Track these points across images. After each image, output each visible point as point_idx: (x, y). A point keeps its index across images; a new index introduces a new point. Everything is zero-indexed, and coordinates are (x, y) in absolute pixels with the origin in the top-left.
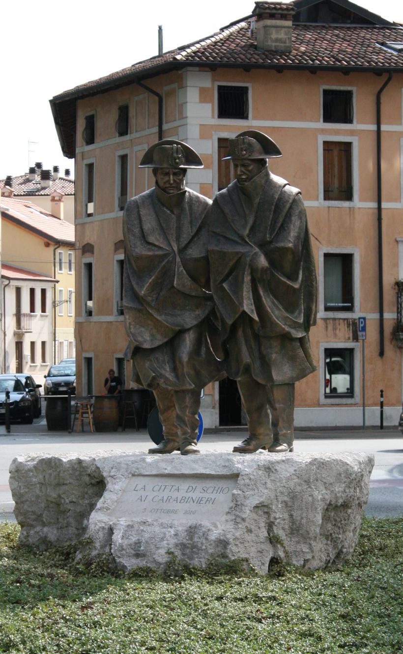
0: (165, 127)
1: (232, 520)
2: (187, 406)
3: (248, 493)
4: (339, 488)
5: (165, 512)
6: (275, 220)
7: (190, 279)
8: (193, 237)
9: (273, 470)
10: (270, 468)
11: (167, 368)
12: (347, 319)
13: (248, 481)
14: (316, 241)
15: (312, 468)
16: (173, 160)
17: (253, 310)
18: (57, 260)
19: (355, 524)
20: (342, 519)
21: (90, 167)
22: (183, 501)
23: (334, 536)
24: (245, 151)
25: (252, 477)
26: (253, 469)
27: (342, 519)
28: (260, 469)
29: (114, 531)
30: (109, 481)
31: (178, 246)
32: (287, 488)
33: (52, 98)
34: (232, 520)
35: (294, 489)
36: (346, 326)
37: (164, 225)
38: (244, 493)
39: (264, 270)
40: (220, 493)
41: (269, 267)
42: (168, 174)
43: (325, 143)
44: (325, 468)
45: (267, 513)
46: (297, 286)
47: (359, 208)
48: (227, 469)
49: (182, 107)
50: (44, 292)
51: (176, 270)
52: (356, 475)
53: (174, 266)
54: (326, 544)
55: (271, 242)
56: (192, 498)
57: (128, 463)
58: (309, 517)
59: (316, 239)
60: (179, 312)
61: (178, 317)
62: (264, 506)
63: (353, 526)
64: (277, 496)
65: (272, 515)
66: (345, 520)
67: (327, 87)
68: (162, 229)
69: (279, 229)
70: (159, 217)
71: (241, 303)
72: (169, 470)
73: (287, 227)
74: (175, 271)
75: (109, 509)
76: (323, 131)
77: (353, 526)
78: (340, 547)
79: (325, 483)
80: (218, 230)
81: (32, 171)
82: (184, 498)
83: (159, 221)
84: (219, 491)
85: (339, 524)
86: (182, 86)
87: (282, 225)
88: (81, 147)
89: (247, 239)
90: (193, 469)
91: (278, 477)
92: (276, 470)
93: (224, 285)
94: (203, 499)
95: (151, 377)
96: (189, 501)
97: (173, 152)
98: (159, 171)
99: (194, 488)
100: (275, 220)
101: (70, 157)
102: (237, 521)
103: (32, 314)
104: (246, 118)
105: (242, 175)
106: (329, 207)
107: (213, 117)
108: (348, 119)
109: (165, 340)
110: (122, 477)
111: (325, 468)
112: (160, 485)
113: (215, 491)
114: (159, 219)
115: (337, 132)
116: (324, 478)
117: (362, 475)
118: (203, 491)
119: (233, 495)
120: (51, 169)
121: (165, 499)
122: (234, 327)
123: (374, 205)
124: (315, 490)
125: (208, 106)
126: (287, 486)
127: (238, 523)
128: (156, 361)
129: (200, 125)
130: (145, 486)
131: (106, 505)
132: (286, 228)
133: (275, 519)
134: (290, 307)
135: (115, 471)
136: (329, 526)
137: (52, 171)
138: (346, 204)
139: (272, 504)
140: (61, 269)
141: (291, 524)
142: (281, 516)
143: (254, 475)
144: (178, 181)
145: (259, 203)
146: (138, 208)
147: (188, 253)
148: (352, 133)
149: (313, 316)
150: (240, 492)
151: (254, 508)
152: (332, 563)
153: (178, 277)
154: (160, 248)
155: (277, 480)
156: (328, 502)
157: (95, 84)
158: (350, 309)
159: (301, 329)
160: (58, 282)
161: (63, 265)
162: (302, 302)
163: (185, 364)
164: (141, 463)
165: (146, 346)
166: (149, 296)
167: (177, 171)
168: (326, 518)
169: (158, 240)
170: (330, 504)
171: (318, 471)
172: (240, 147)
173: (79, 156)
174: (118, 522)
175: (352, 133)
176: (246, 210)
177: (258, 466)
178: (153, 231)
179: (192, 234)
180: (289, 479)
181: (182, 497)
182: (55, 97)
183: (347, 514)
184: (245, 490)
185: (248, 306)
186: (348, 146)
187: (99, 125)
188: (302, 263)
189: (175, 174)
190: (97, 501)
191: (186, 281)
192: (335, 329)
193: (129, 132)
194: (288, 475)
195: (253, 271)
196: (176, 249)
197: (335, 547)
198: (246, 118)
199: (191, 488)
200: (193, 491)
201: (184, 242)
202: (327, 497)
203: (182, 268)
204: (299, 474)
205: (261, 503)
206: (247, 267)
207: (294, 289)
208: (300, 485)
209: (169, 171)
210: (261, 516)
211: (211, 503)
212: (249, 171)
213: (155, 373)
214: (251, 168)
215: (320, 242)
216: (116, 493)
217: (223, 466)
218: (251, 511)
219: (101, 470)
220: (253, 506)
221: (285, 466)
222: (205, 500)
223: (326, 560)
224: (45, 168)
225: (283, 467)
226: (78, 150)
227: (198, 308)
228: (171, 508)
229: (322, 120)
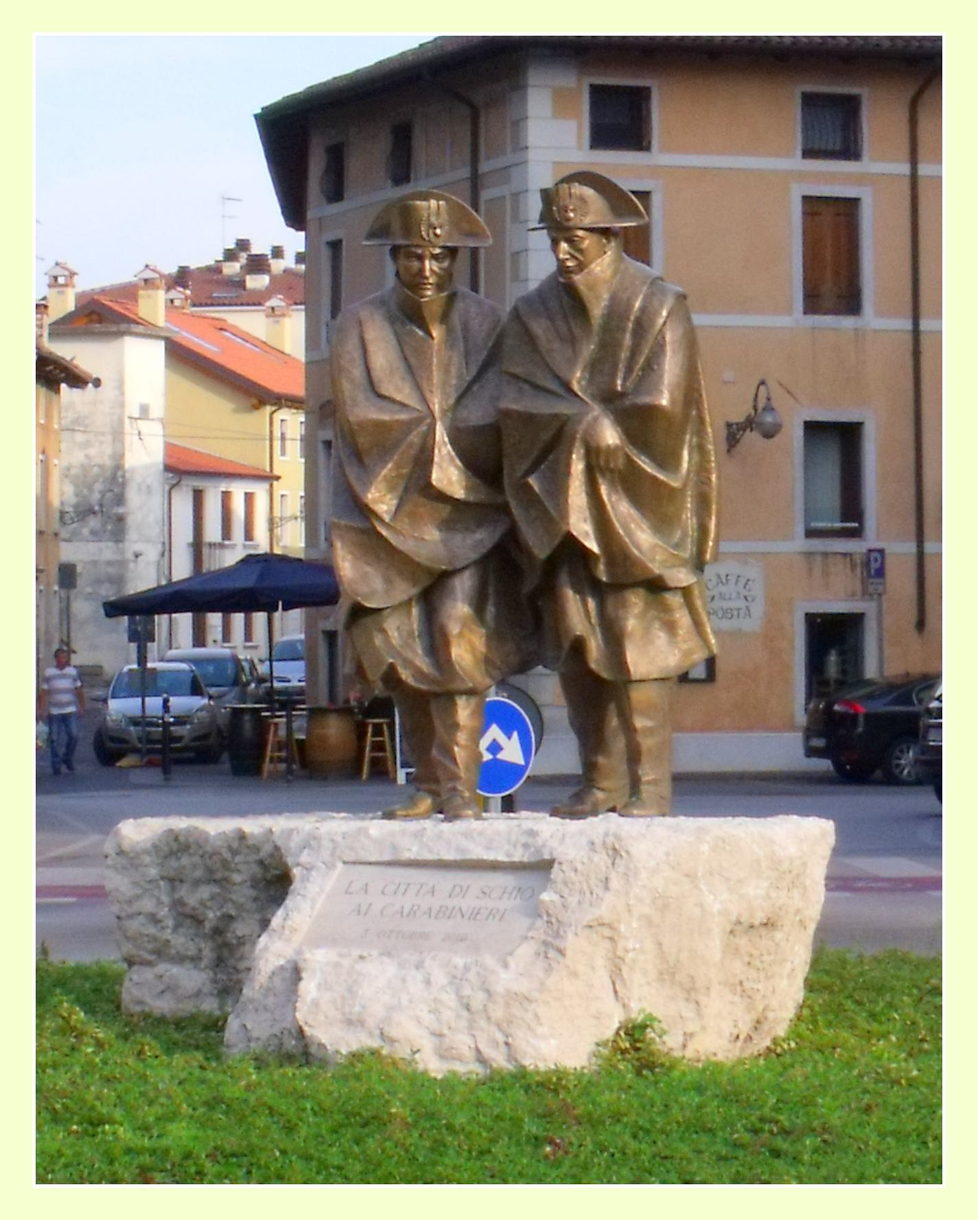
0: (484, 167)
4: (756, 890)
12: (851, 555)
14: (787, 395)
16: (431, 231)
18: (277, 434)
19: (792, 962)
20: (765, 952)
21: (335, 246)
22: (441, 915)
23: (747, 985)
24: (572, 210)
27: (765, 952)
29: (304, 975)
33: (259, 111)
36: (849, 566)
37: (413, 361)
39: (610, 451)
43: (807, 199)
44: (728, 848)
45: (611, 939)
46: (675, 484)
47: (875, 331)
49: (519, 124)
50: (249, 498)
52: (791, 864)
54: (732, 1003)
59: (789, 392)
63: (788, 966)
66: (769, 954)
67: (599, 81)
68: (410, 369)
69: (643, 369)
72: (413, 851)
76: (801, 176)
77: (788, 966)
78: (760, 1008)
79: (728, 880)
80: (518, 370)
81: (230, 255)
85: (758, 963)
86: (520, 87)
88: (316, 207)
90: (463, 851)
93: (532, 481)
94: (482, 911)
98: (402, 251)
101: (298, 229)
103: (227, 542)
104: (648, 148)
106: (814, 328)
107: (580, 147)
108: (850, 151)
111: (728, 848)
113: (506, 895)
115: (832, 178)
117: (804, 864)
118: (481, 895)
120: (268, 252)
121: (406, 911)
122: (552, 566)
123: (907, 325)
125: (572, 124)
129: (554, 163)
130: (367, 885)
132: (655, 367)
133: (627, 951)
134: (662, 521)
136: (738, 966)
137: (270, 257)
138: (847, 322)
140: (283, 453)
148: (860, 179)
152: (745, 1041)
154: (404, 406)
156: (734, 918)
157: (345, 82)
158: (856, 533)
160: (278, 478)
161: (288, 444)
168: (731, 950)
170: (739, 923)
173: (312, 225)
175: (860, 179)
179: (468, 379)
182: (267, 108)
183: (773, 941)
185: (582, 527)
186: (852, 204)
187: (354, 166)
190: (273, 914)
192: (826, 574)
193: (412, 176)
195: (594, 455)
197: (750, 1008)
198: (648, 148)
199: (458, 889)
205: (597, 920)
207: (672, 489)
211: (498, 917)
215: (796, 400)
219: (283, 851)
222: (484, 913)
223: (731, 1034)
224: (255, 250)
226: (311, 214)
229: (799, 153)
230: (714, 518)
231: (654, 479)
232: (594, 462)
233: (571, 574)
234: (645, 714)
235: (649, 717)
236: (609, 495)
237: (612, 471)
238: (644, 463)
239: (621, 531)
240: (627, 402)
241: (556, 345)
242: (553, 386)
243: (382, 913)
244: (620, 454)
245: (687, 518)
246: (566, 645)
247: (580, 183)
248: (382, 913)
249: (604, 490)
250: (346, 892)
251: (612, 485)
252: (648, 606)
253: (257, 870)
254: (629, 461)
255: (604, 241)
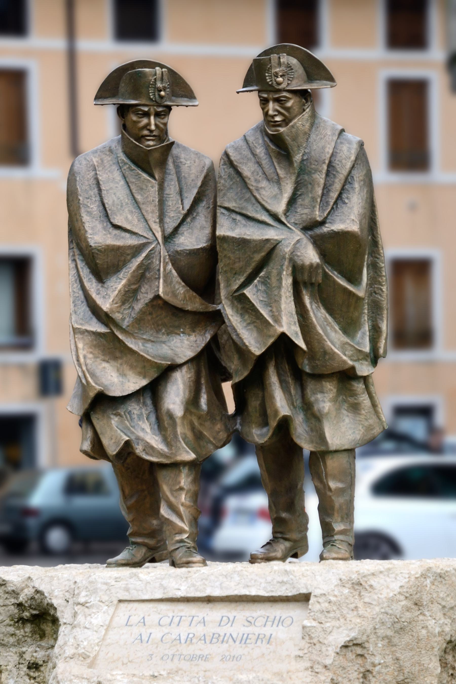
1: (307, 669)
2: (181, 489)
3: (328, 625)
5: (187, 658)
6: (326, 189)
7: (183, 284)
8: (186, 216)
9: (367, 588)
10: (361, 584)
11: (146, 426)
13: (327, 605)
15: (425, 583)
17: (297, 333)
24: (281, 76)
25: (333, 599)
26: (332, 587)
28: (344, 586)
30: (79, 612)
31: (163, 231)
32: (391, 615)
34: (307, 669)
35: (401, 617)
38: (322, 625)
39: (312, 268)
40: (278, 626)
41: (320, 263)
42: (147, 114)
48: (288, 586)
51: (162, 269)
53: (158, 263)
55: (323, 223)
56: (231, 635)
57: (109, 581)
58: (422, 662)
60: (164, 338)
61: (164, 345)
62: (357, 645)
64: (375, 629)
65: (369, 660)
69: (336, 203)
70: (130, 185)
71: (277, 320)
73: (347, 198)
74: (159, 270)
75: (89, 657)
79: (444, 607)
82: (217, 635)
83: (131, 191)
84: (276, 622)
87: (340, 196)
89: (283, 219)
91: (376, 597)
92: (371, 586)
93: (249, 292)
94: (250, 636)
95: (123, 442)
96: (226, 638)
97: (155, 79)
99: (231, 619)
100: (326, 189)
102: (317, 670)
105: (275, 115)
109: (144, 382)
110: (101, 604)
111: (444, 582)
112: (171, 615)
113: (269, 623)
114: (129, 186)
116: (443, 599)
118: (247, 624)
119: (304, 627)
121: (183, 638)
124: (429, 618)
126: (390, 612)
127: (317, 673)
128: (128, 416)
131: (83, 651)
132: (346, 201)
133: (374, 666)
135: (87, 596)
139: (368, 642)
141: (396, 673)
142: (382, 661)
143: (336, 596)
144: (162, 126)
145: (303, 160)
146: (95, 170)
147: (177, 242)
149: (384, 341)
150: (314, 624)
151: (341, 648)
153: (165, 281)
155: (374, 603)
159: (367, 363)
162: (366, 319)
163: (178, 421)
164: (132, 580)
165: (116, 392)
166: (119, 312)
167: (160, 109)
169: (130, 222)
171: (433, 587)
172: (273, 71)
174: (113, 678)
176: (279, 171)
177: (340, 580)
178: (122, 206)
179: (185, 212)
180: (391, 600)
181: (214, 634)
184: (323, 619)
188: (366, 256)
189: (157, 115)
191: (177, 287)
194: (391, 594)
196: (159, 235)
200: (230, 624)
201: (170, 225)
202: (447, 629)
203: (170, 266)
204: (407, 592)
206: (286, 263)
208: (408, 609)
209: (149, 110)
210: (352, 661)
212: (287, 109)
213: (128, 436)
214: (289, 104)
216: (96, 632)
217: (278, 582)
218: (338, 653)
220: (340, 646)
221: (386, 581)
222: (254, 638)
225: (382, 581)
227: (194, 331)
228: (198, 653)
230: (385, 322)
231: (345, 289)
232: (299, 278)
233: (277, 368)
234: (335, 478)
235: (341, 481)
236: (311, 303)
237: (312, 284)
238: (338, 277)
239: (321, 331)
240: (325, 229)
241: (264, 184)
242: (265, 217)
243: (162, 641)
244: (320, 271)
245: (365, 320)
246: (274, 424)
247: (288, 54)
248: (162, 641)
249: (307, 300)
250: (126, 625)
251: (312, 297)
252: (340, 392)
253: (14, 610)
254: (326, 275)
255: (304, 100)
